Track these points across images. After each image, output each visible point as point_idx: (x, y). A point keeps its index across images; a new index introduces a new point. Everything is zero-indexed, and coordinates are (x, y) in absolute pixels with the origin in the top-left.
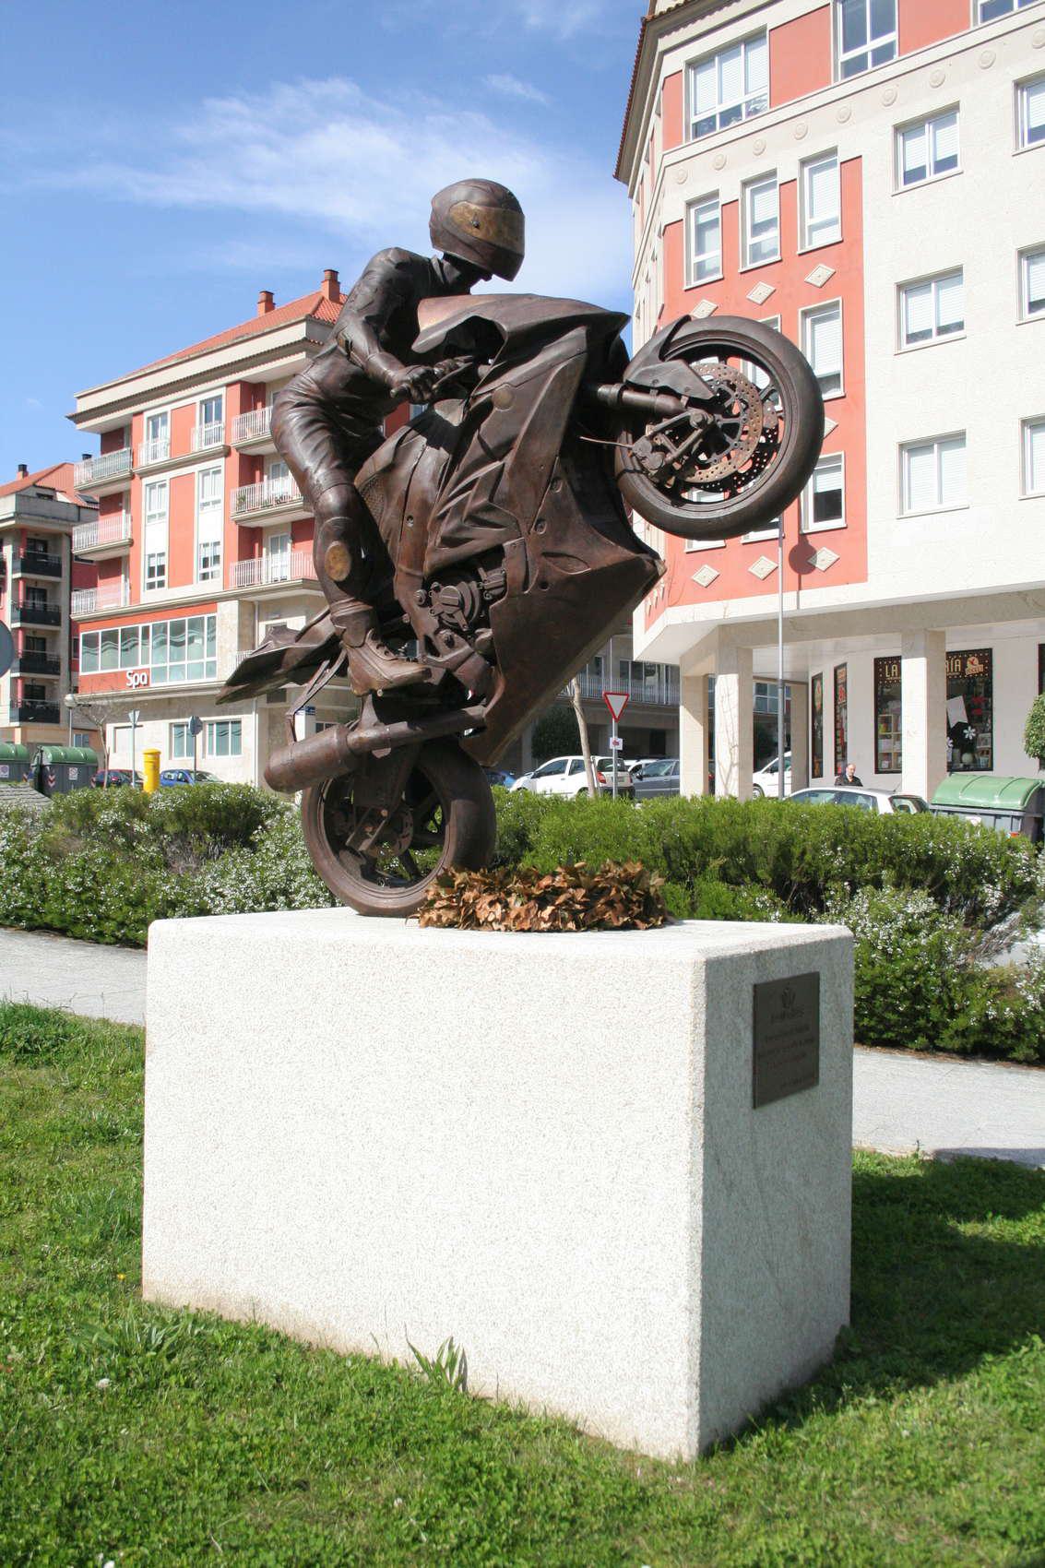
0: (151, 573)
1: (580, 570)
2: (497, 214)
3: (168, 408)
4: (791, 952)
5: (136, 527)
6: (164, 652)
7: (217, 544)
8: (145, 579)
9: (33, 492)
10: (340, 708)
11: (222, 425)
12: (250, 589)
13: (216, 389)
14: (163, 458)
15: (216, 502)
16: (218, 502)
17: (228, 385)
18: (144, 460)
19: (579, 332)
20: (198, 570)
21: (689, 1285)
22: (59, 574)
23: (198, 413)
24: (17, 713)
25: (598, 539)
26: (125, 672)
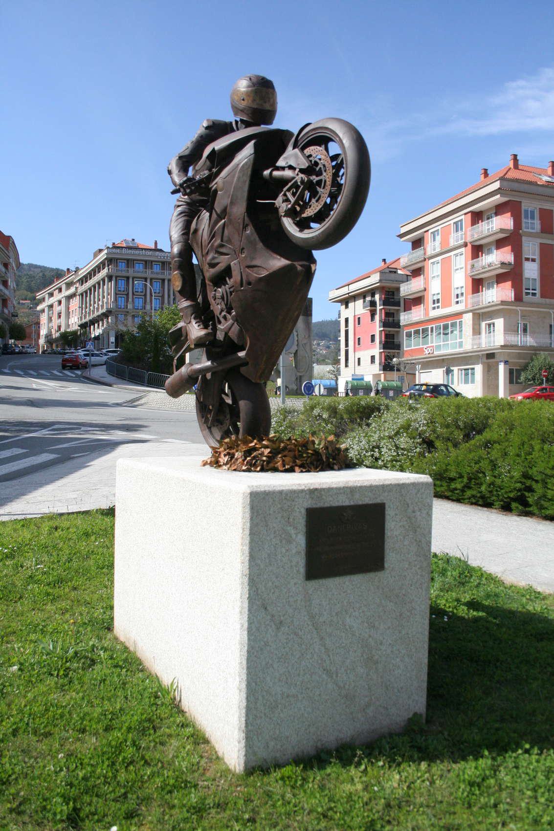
0: (434, 303)
1: (264, 273)
2: (252, 91)
3: (439, 228)
4: (371, 488)
5: (426, 281)
6: (440, 338)
7: (462, 287)
8: (431, 305)
9: (387, 270)
10: (521, 361)
11: (463, 233)
12: (477, 307)
13: (460, 216)
14: (438, 250)
15: (461, 268)
16: (462, 268)
17: (465, 214)
18: (430, 251)
19: (251, 144)
20: (454, 300)
21: (240, 676)
22: (399, 306)
23: (452, 228)
24: (382, 368)
25: (272, 256)
26: (423, 348)
